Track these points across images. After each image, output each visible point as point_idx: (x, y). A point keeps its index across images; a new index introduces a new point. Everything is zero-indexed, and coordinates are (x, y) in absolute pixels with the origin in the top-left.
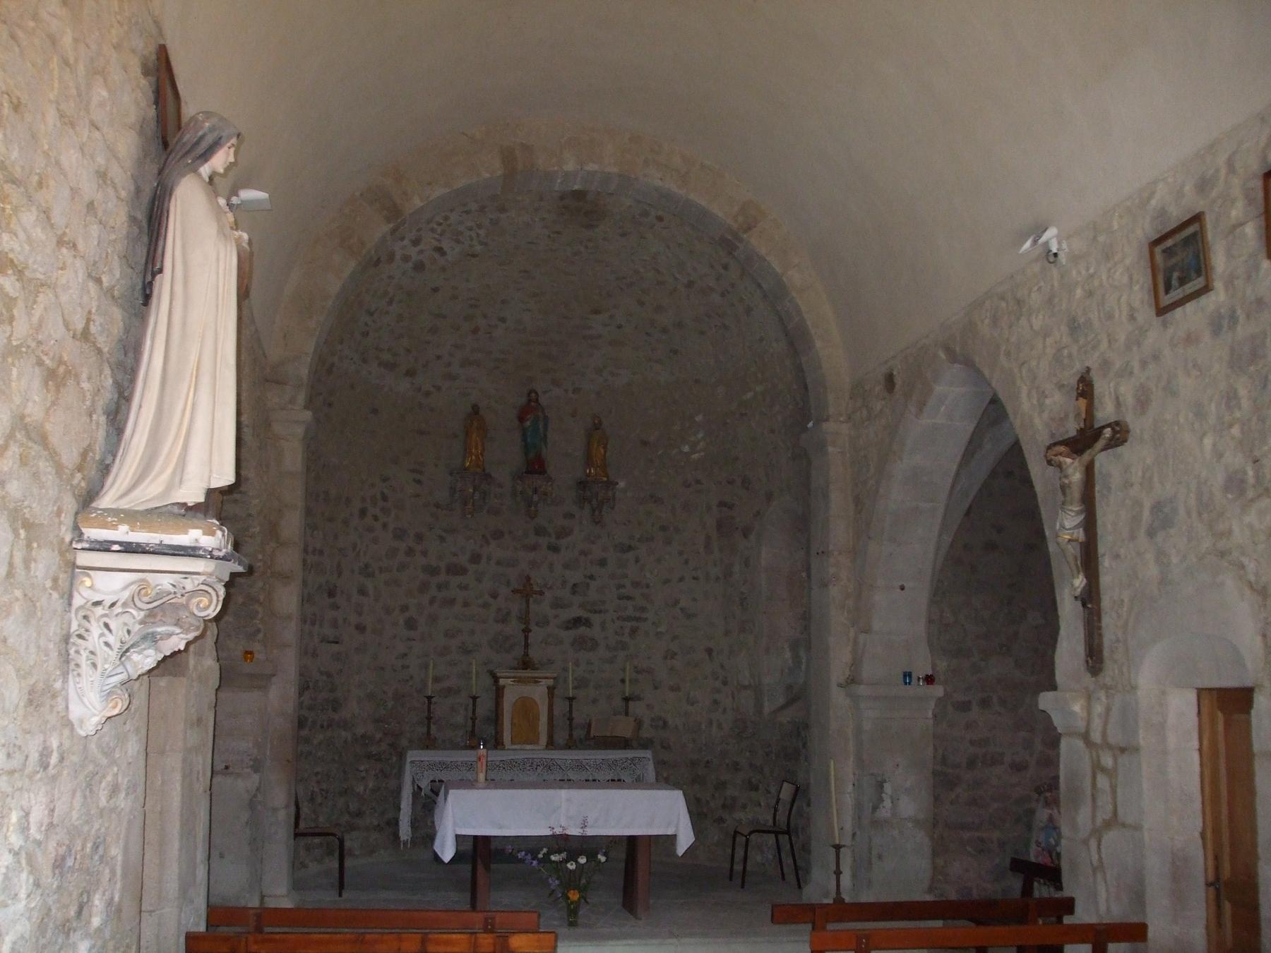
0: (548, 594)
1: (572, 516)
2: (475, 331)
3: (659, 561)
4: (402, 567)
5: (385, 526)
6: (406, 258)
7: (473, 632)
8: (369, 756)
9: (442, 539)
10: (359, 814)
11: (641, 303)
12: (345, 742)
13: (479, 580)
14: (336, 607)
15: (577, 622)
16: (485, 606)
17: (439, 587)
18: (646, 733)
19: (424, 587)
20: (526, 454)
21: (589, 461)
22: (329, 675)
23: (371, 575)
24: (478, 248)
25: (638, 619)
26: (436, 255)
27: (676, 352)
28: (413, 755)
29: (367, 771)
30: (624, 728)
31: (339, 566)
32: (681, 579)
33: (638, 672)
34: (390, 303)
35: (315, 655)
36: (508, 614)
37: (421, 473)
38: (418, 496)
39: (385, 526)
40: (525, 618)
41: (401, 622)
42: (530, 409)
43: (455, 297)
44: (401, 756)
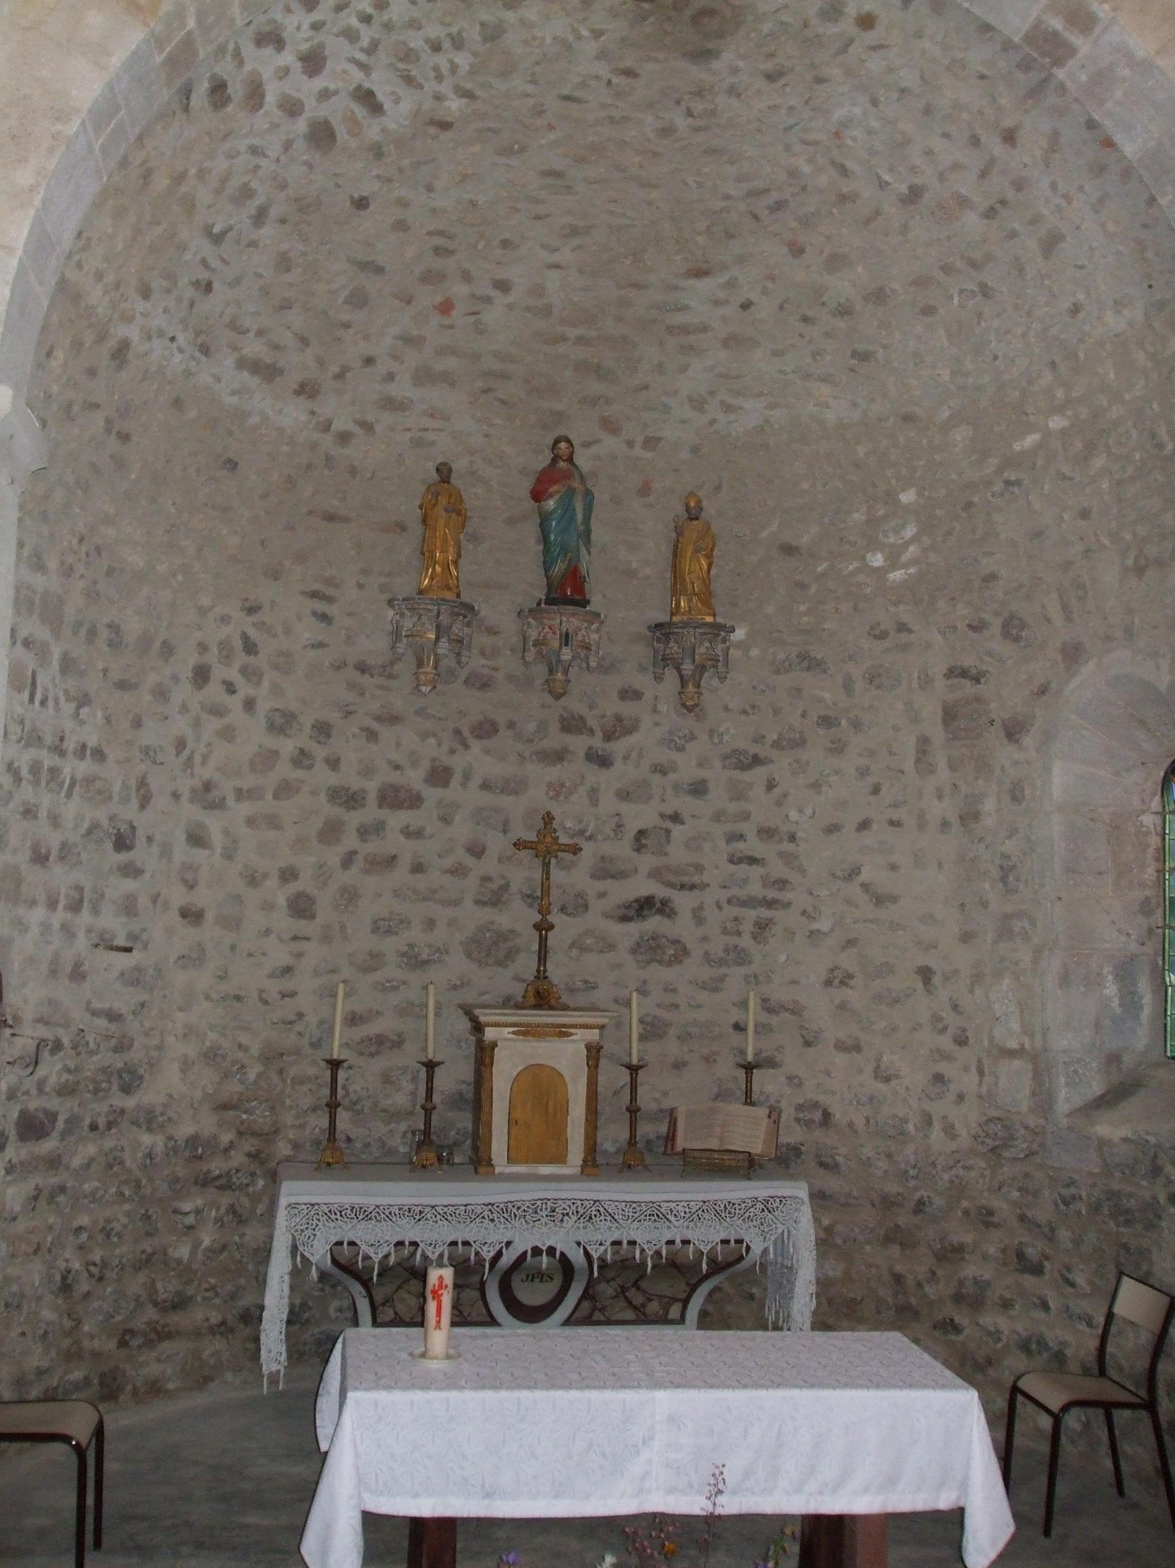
0: (588, 849)
1: (637, 695)
2: (446, 307)
3: (816, 786)
4: (285, 790)
5: (249, 705)
6: (292, 108)
7: (430, 924)
8: (205, 1181)
9: (372, 735)
10: (180, 1303)
11: (797, 251)
12: (150, 1156)
13: (446, 820)
14: (131, 871)
15: (644, 906)
16: (458, 871)
17: (364, 832)
18: (792, 1135)
19: (331, 832)
20: (547, 566)
21: (677, 585)
22: (113, 1017)
23: (218, 805)
24: (455, 105)
25: (770, 904)
26: (360, 112)
27: (864, 357)
28: (294, 1192)
29: (198, 1212)
30: (747, 1132)
31: (142, 783)
32: (864, 825)
33: (770, 1010)
34: (260, 217)
35: (78, 974)
36: (506, 887)
37: (330, 600)
38: (321, 645)
39: (249, 705)
40: (540, 899)
41: (282, 901)
42: (556, 475)
43: (401, 226)
44: (274, 1178)
